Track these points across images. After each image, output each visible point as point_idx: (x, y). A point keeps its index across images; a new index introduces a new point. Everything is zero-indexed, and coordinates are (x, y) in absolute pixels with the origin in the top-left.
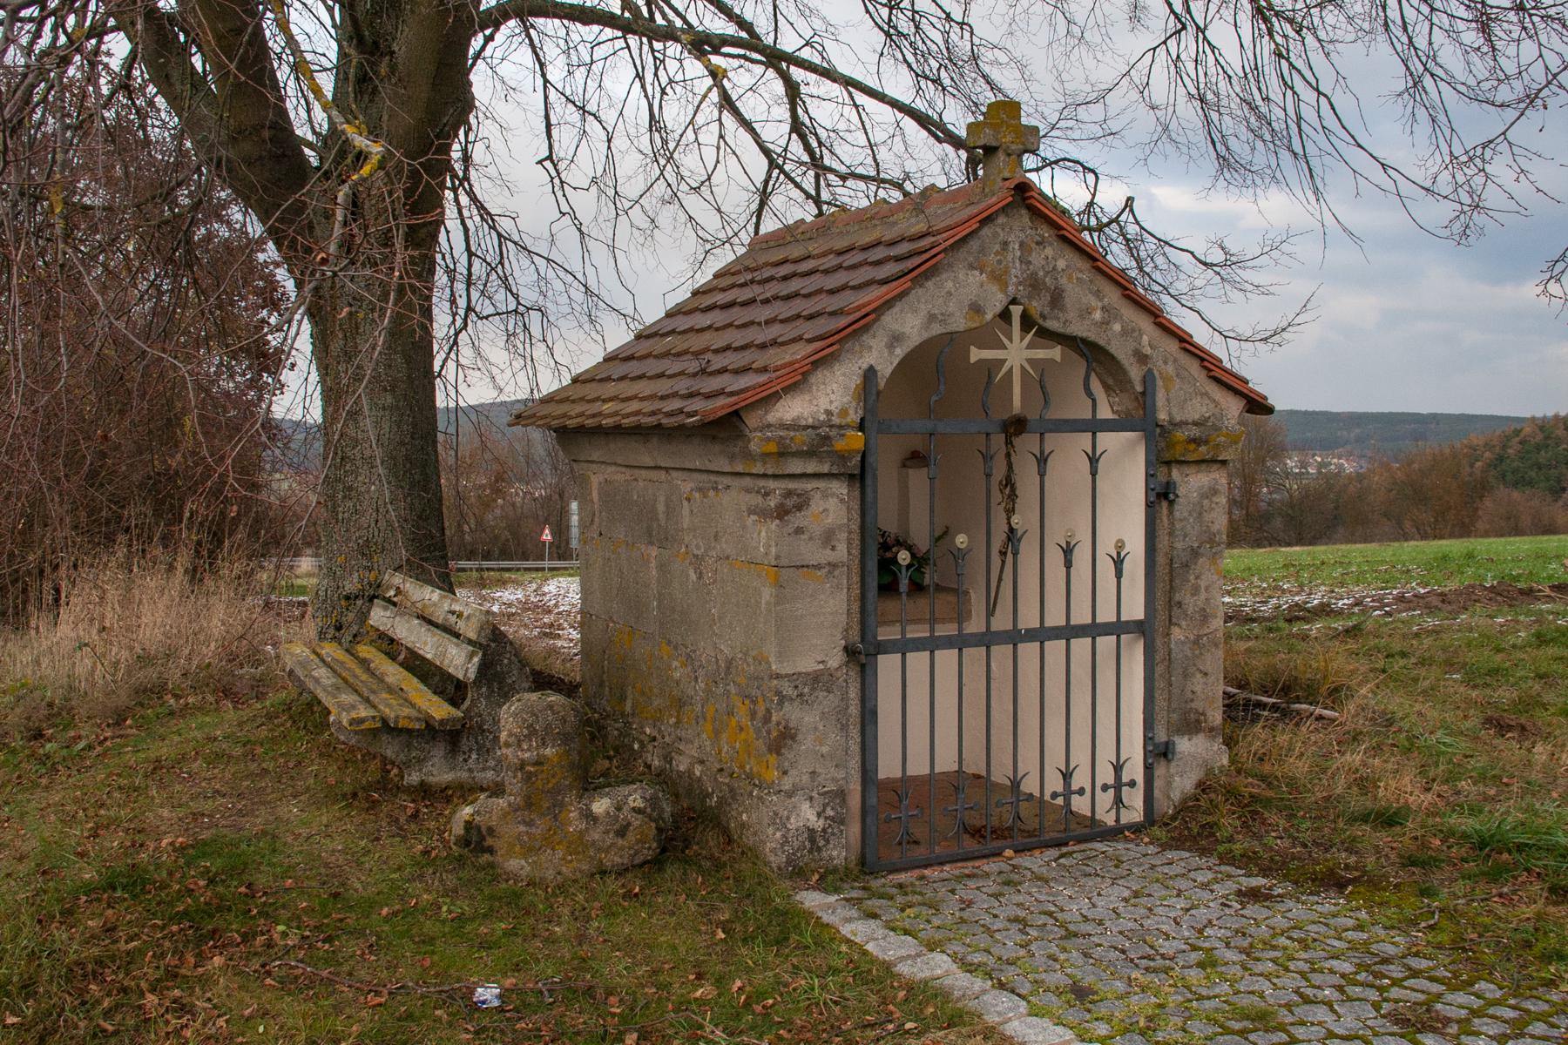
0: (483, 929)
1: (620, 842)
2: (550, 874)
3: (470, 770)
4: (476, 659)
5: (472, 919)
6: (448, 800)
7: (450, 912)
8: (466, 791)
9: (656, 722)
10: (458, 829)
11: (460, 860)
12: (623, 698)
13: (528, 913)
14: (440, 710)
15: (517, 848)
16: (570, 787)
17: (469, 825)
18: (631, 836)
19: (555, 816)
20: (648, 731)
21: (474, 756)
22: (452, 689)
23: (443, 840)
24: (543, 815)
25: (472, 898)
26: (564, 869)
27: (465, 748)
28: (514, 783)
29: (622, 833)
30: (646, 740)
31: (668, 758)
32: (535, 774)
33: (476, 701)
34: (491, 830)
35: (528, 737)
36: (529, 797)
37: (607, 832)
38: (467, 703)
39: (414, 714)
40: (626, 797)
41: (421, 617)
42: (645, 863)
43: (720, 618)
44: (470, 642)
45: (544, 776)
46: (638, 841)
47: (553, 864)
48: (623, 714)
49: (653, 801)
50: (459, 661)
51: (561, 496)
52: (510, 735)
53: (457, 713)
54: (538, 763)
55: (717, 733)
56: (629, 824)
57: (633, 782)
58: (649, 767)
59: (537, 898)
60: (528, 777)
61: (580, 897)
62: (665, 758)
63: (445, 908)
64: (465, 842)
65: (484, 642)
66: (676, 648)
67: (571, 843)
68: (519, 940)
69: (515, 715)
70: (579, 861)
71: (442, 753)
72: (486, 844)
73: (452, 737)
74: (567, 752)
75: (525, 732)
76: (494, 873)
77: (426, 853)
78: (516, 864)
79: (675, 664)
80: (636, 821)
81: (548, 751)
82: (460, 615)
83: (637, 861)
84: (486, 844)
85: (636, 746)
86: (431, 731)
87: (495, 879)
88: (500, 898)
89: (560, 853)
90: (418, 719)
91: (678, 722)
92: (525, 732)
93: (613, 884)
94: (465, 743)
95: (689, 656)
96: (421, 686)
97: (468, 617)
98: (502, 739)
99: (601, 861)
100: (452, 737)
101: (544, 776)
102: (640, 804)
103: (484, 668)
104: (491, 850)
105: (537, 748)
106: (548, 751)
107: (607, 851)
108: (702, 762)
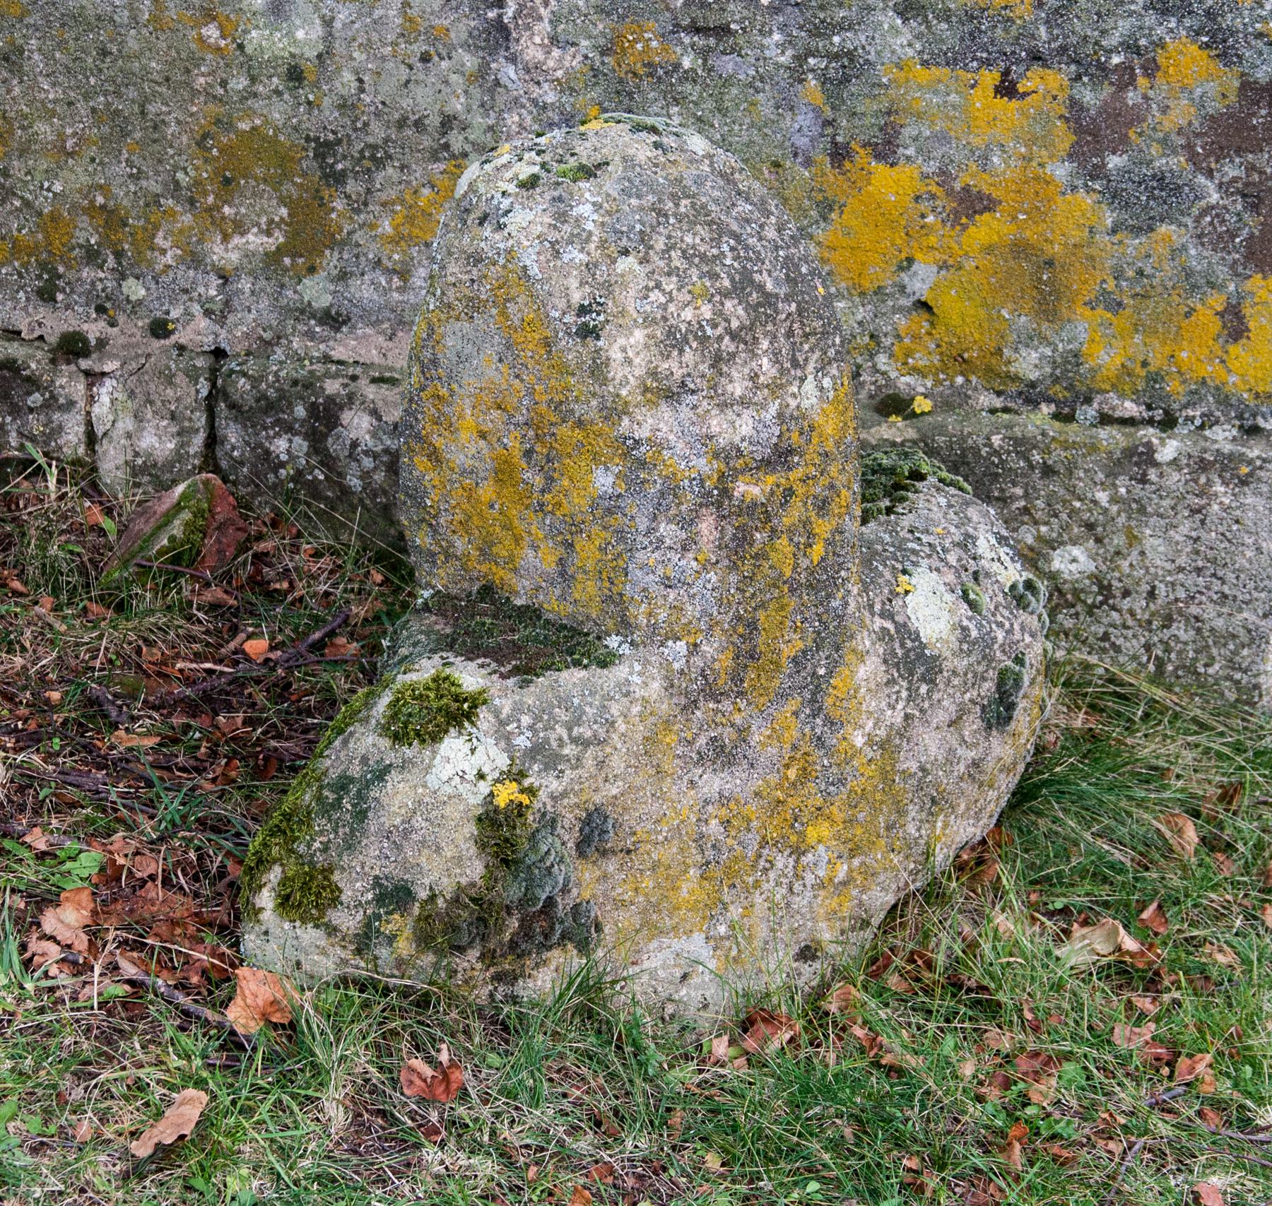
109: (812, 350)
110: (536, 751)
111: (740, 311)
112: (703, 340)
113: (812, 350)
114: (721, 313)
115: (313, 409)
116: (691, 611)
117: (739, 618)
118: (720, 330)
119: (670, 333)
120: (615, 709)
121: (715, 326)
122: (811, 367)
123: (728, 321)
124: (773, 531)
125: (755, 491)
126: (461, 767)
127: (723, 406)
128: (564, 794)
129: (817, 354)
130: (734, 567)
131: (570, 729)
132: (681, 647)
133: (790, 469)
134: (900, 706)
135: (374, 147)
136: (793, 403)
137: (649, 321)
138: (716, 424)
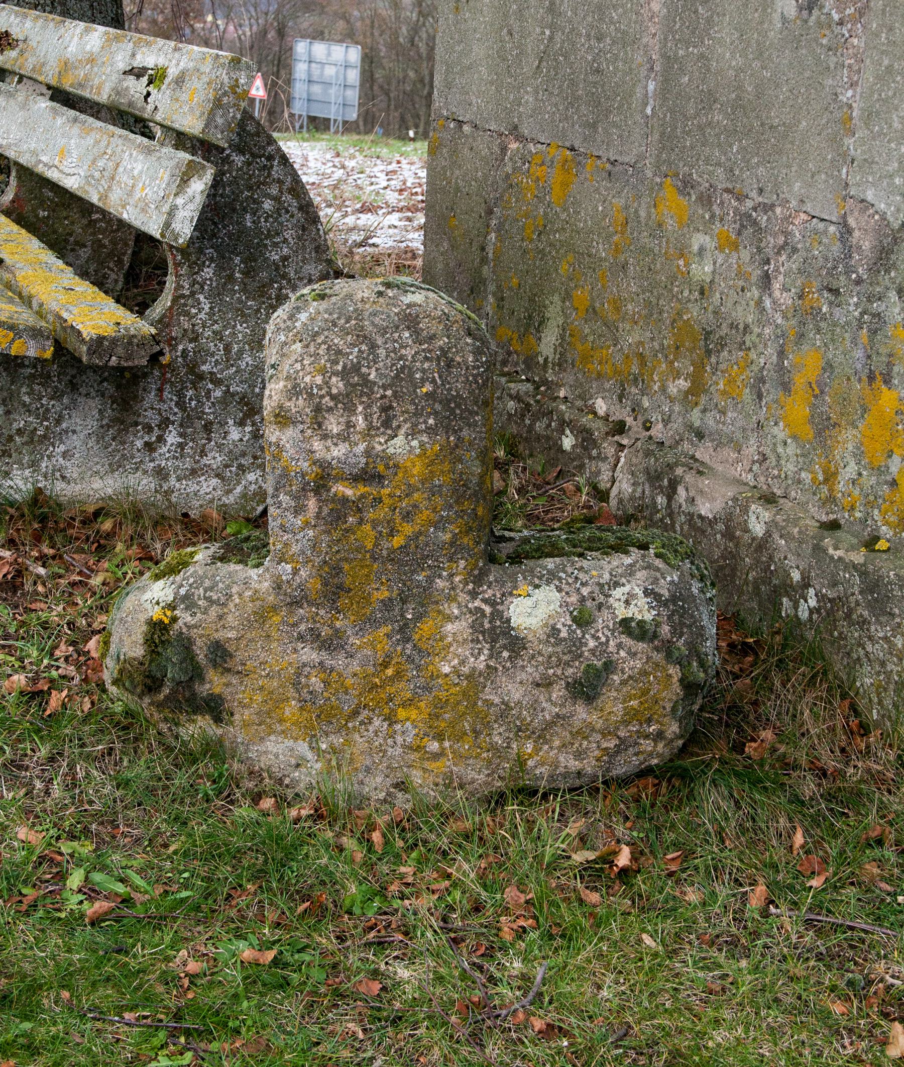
0: (186, 962)
1: (582, 713)
2: (376, 786)
3: (161, 473)
4: (198, 187)
5: (157, 922)
6: (102, 547)
7: (90, 892)
8: (159, 531)
9: (630, 381)
10: (129, 642)
11: (128, 725)
12: (533, 323)
13: (318, 912)
14: (94, 314)
15: (291, 709)
16: (454, 549)
17: (158, 634)
18: (613, 703)
19: (404, 631)
20: (601, 406)
21: (172, 438)
22: (127, 262)
23: (81, 659)
24: (373, 622)
25: (156, 843)
26: (417, 778)
27: (151, 417)
28: (294, 529)
29: (586, 689)
30: (598, 429)
31: (663, 479)
32: (357, 507)
33: (189, 301)
34: (220, 653)
35: (345, 401)
36: (337, 570)
37: (545, 684)
38: (164, 302)
39: (25, 318)
40: (605, 589)
41: (62, 97)
42: (645, 773)
43: (869, 116)
44: (181, 140)
45: (382, 513)
46: (630, 716)
47: (389, 761)
48: (530, 362)
49: (676, 604)
50: (152, 192)
51: (281, 33)
52: (295, 391)
53: (140, 326)
54: (366, 476)
55: (824, 428)
56: (609, 666)
57: (620, 548)
58: (602, 496)
59: (336, 859)
60: (337, 514)
61: (465, 869)
62: (654, 478)
63: (75, 880)
64: (146, 678)
65: (219, 138)
66: (706, 200)
67: (440, 705)
68: (292, 1007)
69: (310, 337)
70: (459, 757)
71: (92, 424)
72: (203, 690)
73: (120, 386)
74: (452, 453)
75: (338, 385)
76: (225, 778)
77: (35, 696)
78: (283, 753)
79: (698, 240)
80: (632, 658)
81: (399, 446)
82: (156, 77)
83: (619, 771)
84: (203, 690)
85: (568, 442)
86: (67, 366)
87: (226, 790)
88: (237, 855)
89: (407, 732)
90: (36, 333)
91: (697, 389)
92: (338, 385)
93: (562, 837)
94: (150, 406)
95: (746, 221)
96: (49, 257)
97: (180, 81)
98: (269, 405)
99: (521, 762)
100: (120, 386)
101: (382, 513)
102: (642, 610)
103: (216, 214)
104: (215, 708)
105: (369, 432)
106: (399, 446)
107: (542, 736)
108: (769, 499)
109: (405, 421)
110: (187, 597)
111: (341, 385)
112: (311, 395)
113: (405, 421)
114: (327, 383)
115: (670, 480)
116: (295, 549)
117: (325, 562)
118: (323, 392)
119: (294, 387)
120: (234, 590)
121: (321, 389)
122: (402, 431)
123: (330, 388)
124: (362, 519)
125: (349, 492)
126: (153, 595)
127: (325, 437)
128: (195, 626)
129: (408, 425)
130: (328, 532)
131: (205, 591)
132: (289, 567)
133: (383, 487)
134: (482, 658)
135: (721, 338)
136: (379, 448)
137: (288, 378)
138: (317, 445)
